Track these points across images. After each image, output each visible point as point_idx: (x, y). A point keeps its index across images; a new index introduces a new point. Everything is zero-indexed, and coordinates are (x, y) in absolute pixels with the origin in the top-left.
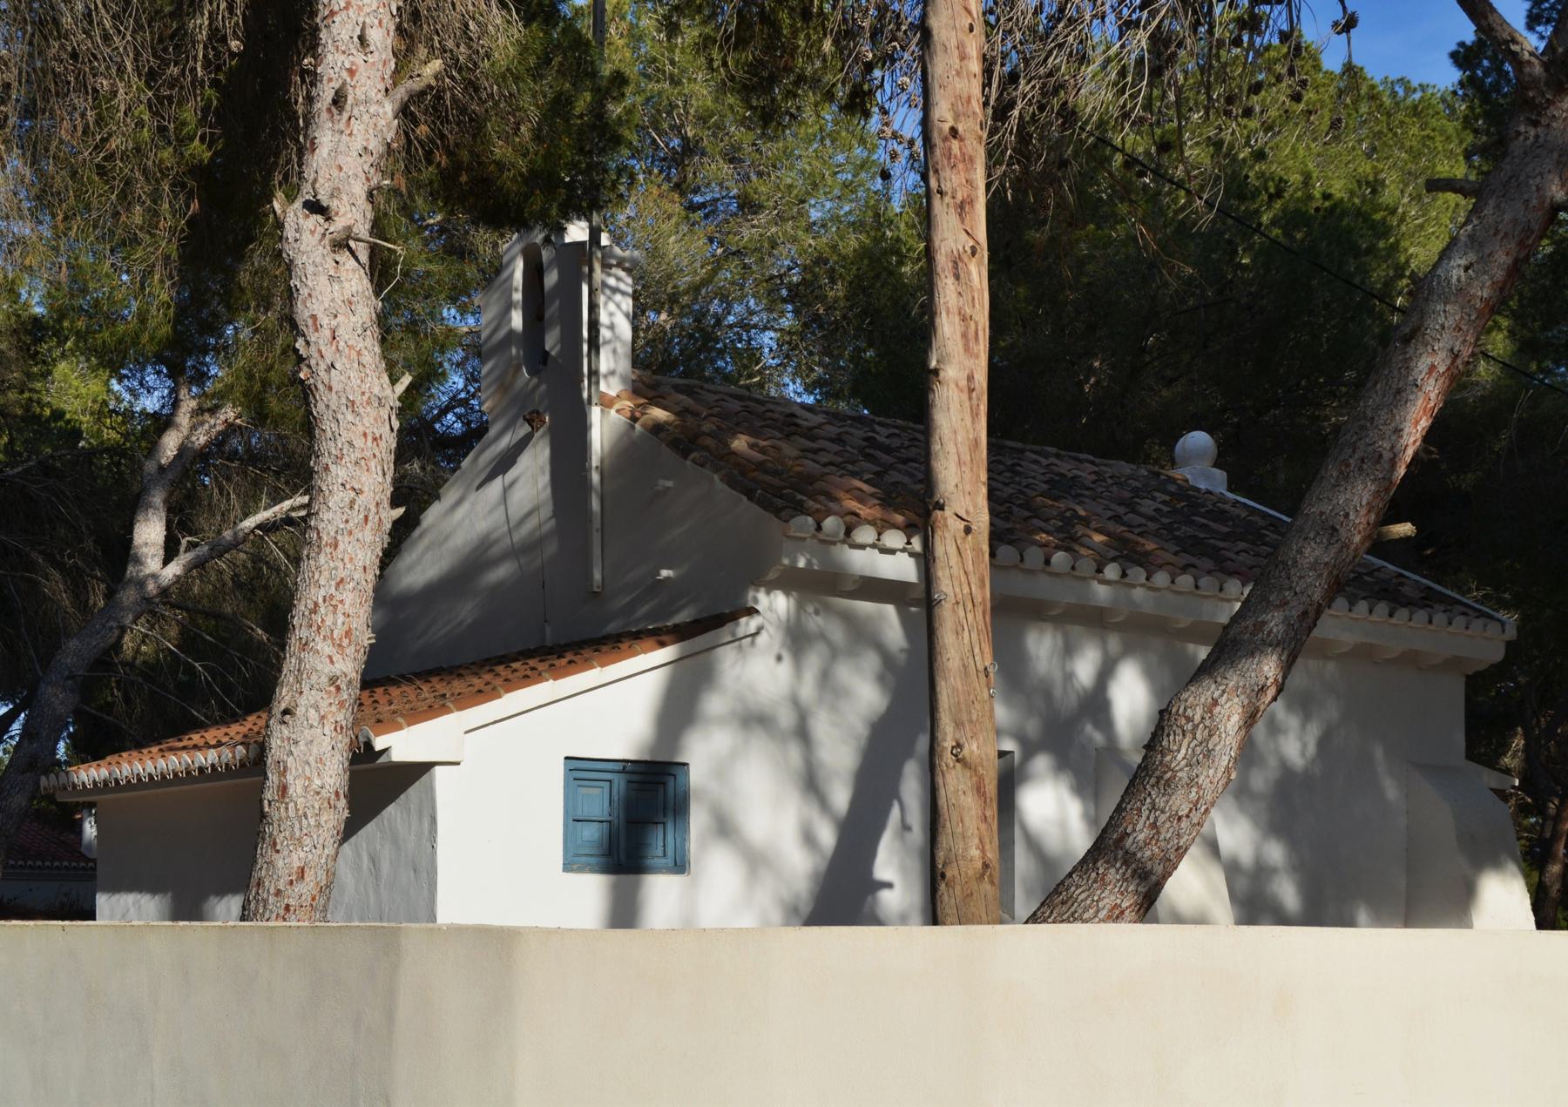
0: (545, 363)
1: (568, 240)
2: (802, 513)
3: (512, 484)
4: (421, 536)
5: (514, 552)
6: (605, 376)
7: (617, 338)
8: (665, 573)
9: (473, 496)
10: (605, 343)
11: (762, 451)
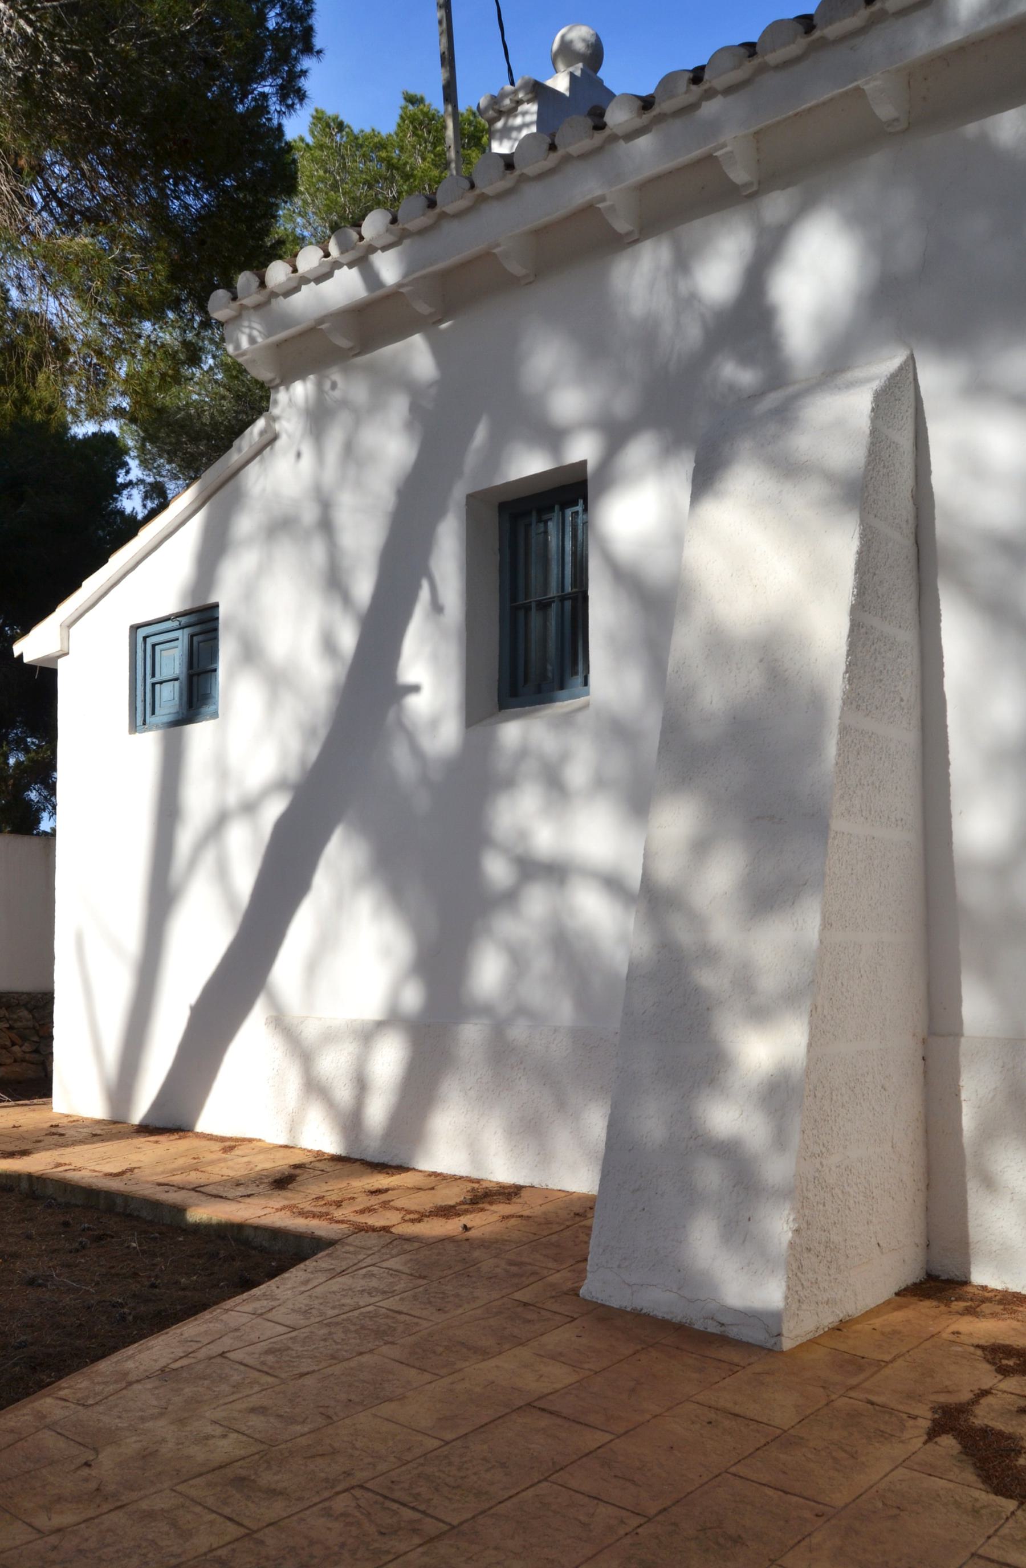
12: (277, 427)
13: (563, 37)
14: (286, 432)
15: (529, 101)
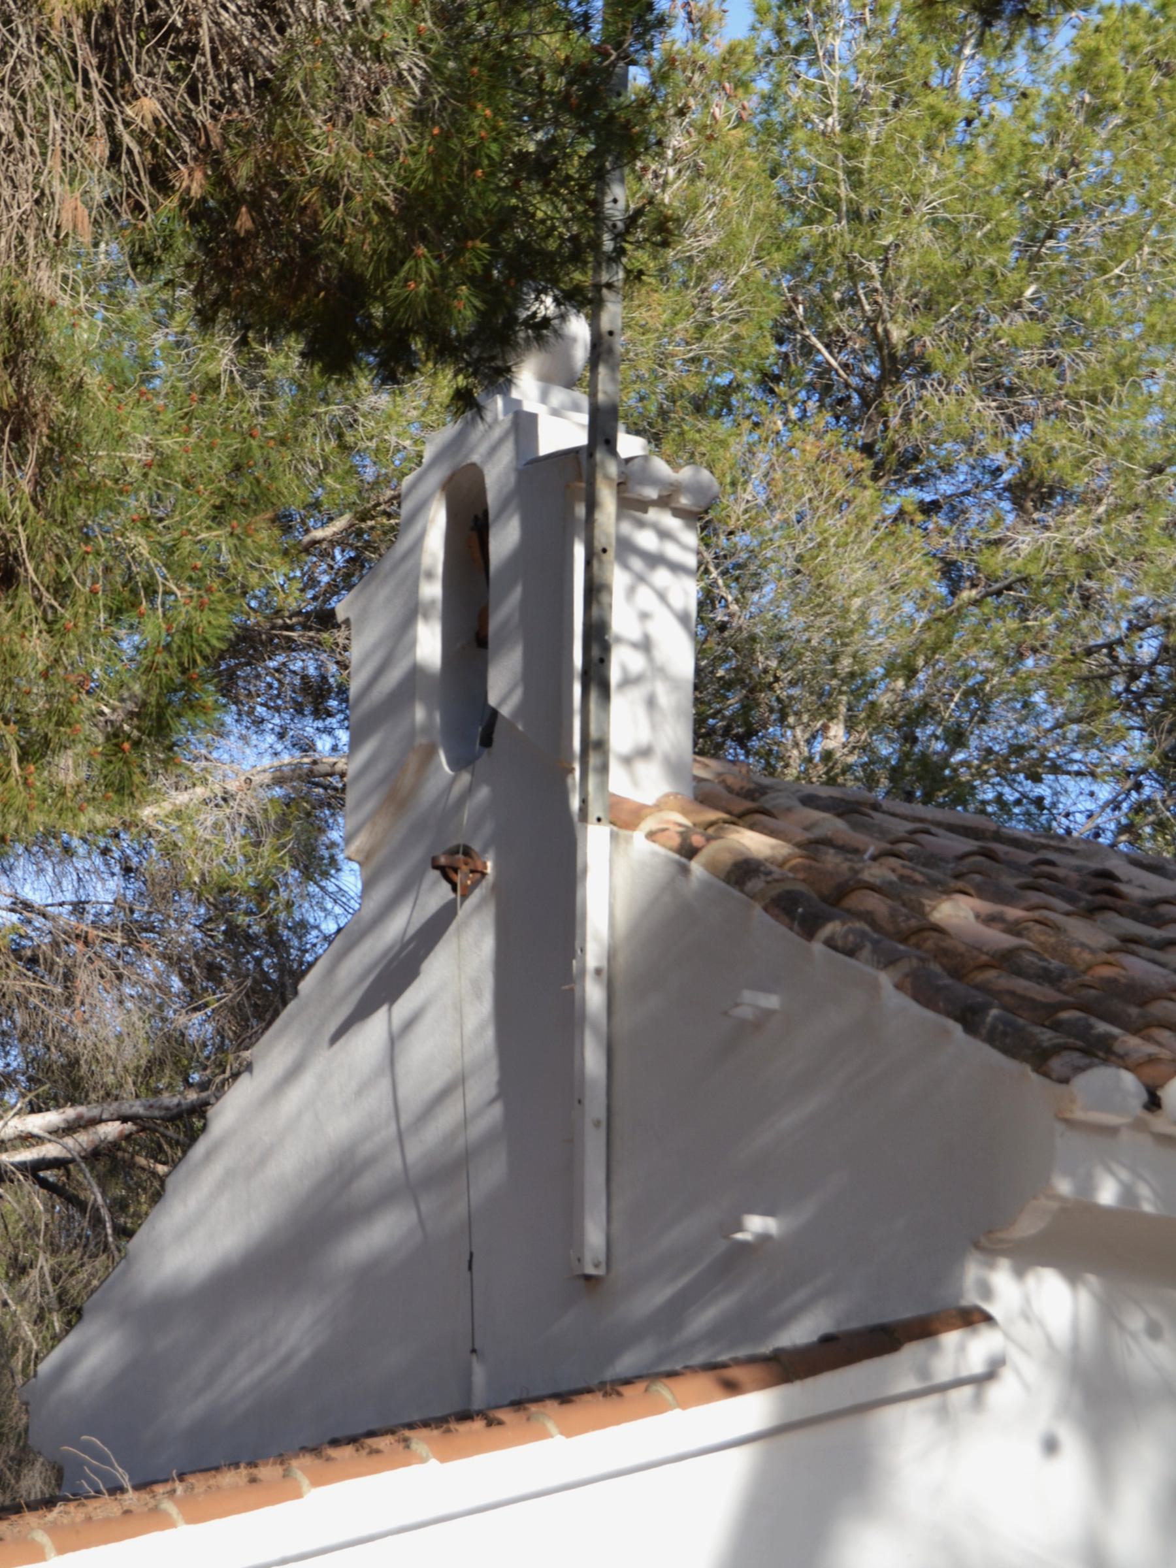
0: (487, 740)
1: (545, 449)
2: (1105, 1061)
3: (410, 1024)
4: (208, 1156)
5: (410, 1187)
6: (627, 761)
7: (659, 671)
8: (756, 1224)
9: (323, 1059)
10: (628, 681)
11: (1014, 929)
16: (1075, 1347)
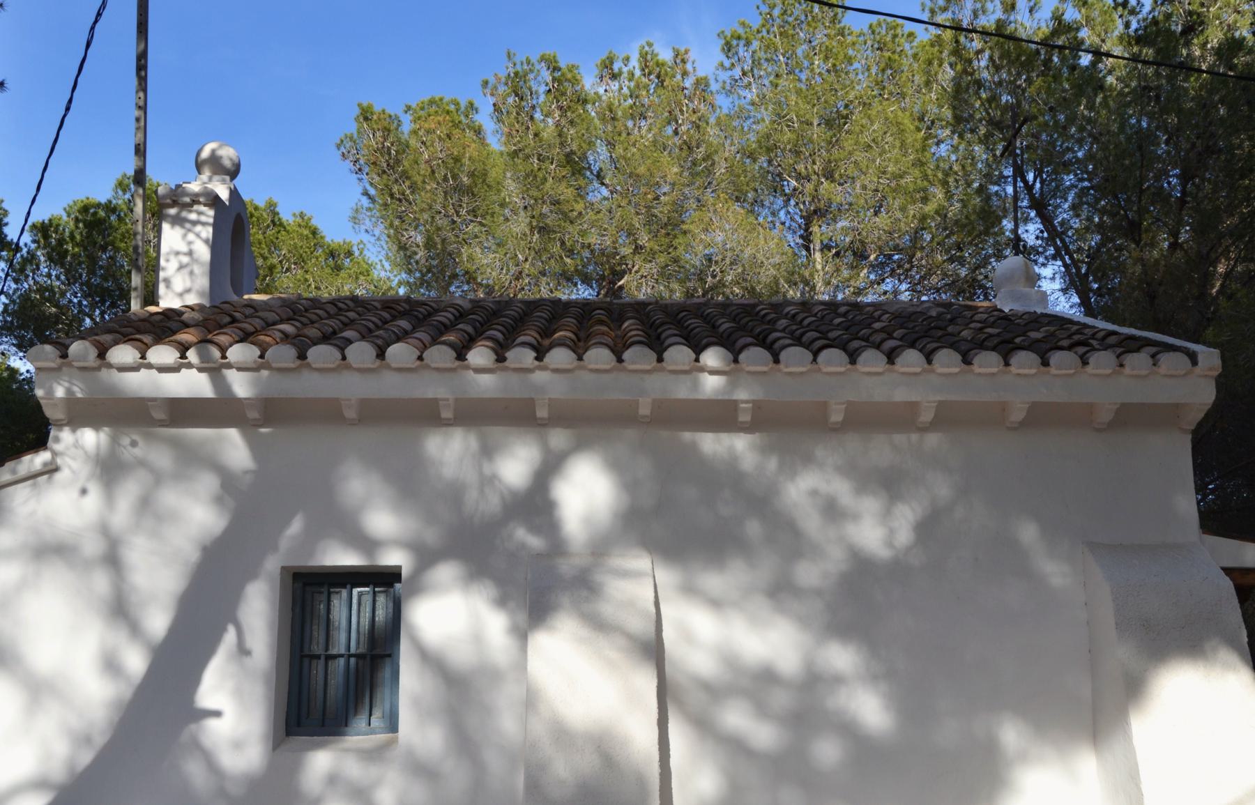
12: (59, 461)
13: (213, 151)
14: (70, 467)
15: (205, 205)
16: (98, 455)
